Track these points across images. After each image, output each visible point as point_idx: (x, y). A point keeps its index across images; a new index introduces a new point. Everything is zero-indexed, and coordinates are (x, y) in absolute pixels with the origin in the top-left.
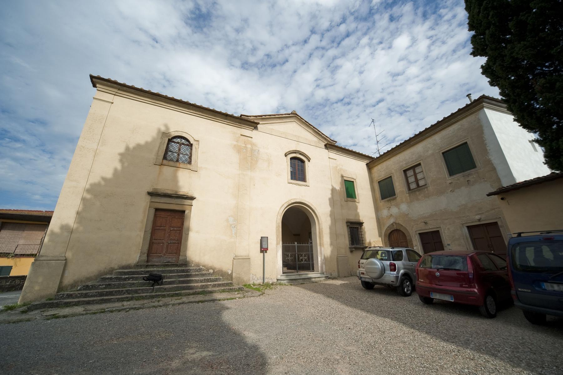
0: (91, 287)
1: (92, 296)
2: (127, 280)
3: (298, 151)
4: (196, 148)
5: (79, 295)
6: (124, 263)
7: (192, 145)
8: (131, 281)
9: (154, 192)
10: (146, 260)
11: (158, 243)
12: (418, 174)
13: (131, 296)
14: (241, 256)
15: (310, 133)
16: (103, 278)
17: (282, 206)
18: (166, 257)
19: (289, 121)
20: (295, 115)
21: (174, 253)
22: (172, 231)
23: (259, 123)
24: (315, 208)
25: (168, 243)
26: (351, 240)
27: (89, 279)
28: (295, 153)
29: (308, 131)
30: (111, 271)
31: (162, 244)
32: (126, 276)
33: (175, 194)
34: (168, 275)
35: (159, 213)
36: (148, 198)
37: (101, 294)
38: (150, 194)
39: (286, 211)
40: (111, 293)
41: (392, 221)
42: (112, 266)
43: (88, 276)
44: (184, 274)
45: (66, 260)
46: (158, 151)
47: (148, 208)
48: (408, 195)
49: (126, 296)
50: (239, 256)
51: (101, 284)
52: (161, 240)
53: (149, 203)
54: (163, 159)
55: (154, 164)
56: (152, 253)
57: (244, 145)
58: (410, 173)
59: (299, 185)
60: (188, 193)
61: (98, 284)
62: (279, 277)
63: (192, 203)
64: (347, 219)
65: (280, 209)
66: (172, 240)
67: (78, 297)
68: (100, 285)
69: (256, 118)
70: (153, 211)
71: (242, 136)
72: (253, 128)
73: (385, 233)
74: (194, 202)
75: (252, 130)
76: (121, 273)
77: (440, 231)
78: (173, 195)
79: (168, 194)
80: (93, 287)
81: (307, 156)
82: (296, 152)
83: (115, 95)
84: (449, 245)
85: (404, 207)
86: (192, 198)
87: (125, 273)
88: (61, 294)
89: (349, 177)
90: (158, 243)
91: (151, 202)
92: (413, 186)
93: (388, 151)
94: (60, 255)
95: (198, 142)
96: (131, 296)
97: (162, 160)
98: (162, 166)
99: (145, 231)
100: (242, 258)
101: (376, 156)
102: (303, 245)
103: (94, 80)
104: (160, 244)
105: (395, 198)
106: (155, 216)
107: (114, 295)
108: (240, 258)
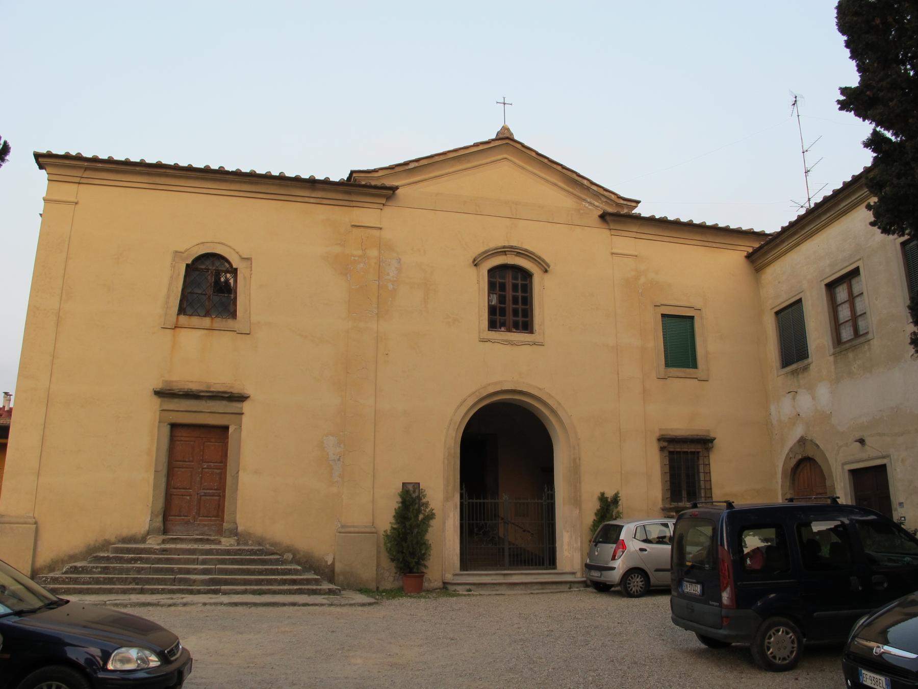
0: (80, 569)
1: (84, 583)
2: (133, 562)
3: (512, 247)
4: (245, 278)
5: (67, 580)
6: (125, 533)
7: (236, 270)
8: (139, 564)
9: (166, 390)
10: (163, 528)
11: (182, 495)
12: (846, 300)
13: (140, 587)
14: (354, 527)
15: (556, 185)
16: (95, 557)
17: (461, 405)
18: (199, 524)
19: (489, 160)
20: (507, 141)
21: (213, 517)
22: (207, 470)
23: (397, 188)
24: (560, 404)
25: (201, 496)
26: (669, 488)
27: (73, 558)
28: (505, 253)
29: (548, 181)
30: (106, 545)
31: (188, 498)
32: (130, 556)
33: (207, 392)
34: (200, 557)
35: (181, 433)
36: (157, 401)
37: (97, 582)
38: (159, 393)
39: (474, 414)
40: (110, 581)
41: (798, 432)
42: (107, 537)
43: (71, 553)
44: (230, 558)
45: (36, 523)
46: (168, 297)
47: (157, 423)
48: (831, 359)
49: (133, 587)
50: (350, 527)
51: (95, 565)
52: (186, 489)
53: (158, 413)
54: (178, 314)
55: (162, 328)
56: (172, 516)
57: (360, 252)
58: (842, 294)
59: (512, 343)
60: (231, 387)
61: (91, 565)
62: (449, 577)
63: (242, 408)
64: (660, 430)
65: (456, 411)
66: (207, 489)
67: (68, 583)
68: (93, 567)
69: (392, 171)
70: (166, 430)
71: (354, 230)
72: (384, 201)
73: (783, 466)
74: (246, 406)
75: (381, 206)
76: (122, 551)
77: (887, 465)
78: (202, 394)
79: (192, 393)
80: (84, 570)
81: (539, 258)
82: (505, 251)
83: (79, 183)
84: (901, 504)
85: (823, 392)
86: (242, 398)
87: (129, 551)
88: (43, 577)
89: (678, 304)
90: (182, 495)
91: (162, 410)
92: (847, 333)
93: (783, 228)
94: (27, 515)
95: (249, 262)
96: (140, 587)
97: (175, 316)
98: (178, 330)
99: (155, 471)
100: (356, 530)
101: (772, 226)
102: (478, 501)
103: (40, 160)
104: (184, 497)
105: (806, 368)
106: (172, 439)
107: (114, 584)
108: (352, 530)
